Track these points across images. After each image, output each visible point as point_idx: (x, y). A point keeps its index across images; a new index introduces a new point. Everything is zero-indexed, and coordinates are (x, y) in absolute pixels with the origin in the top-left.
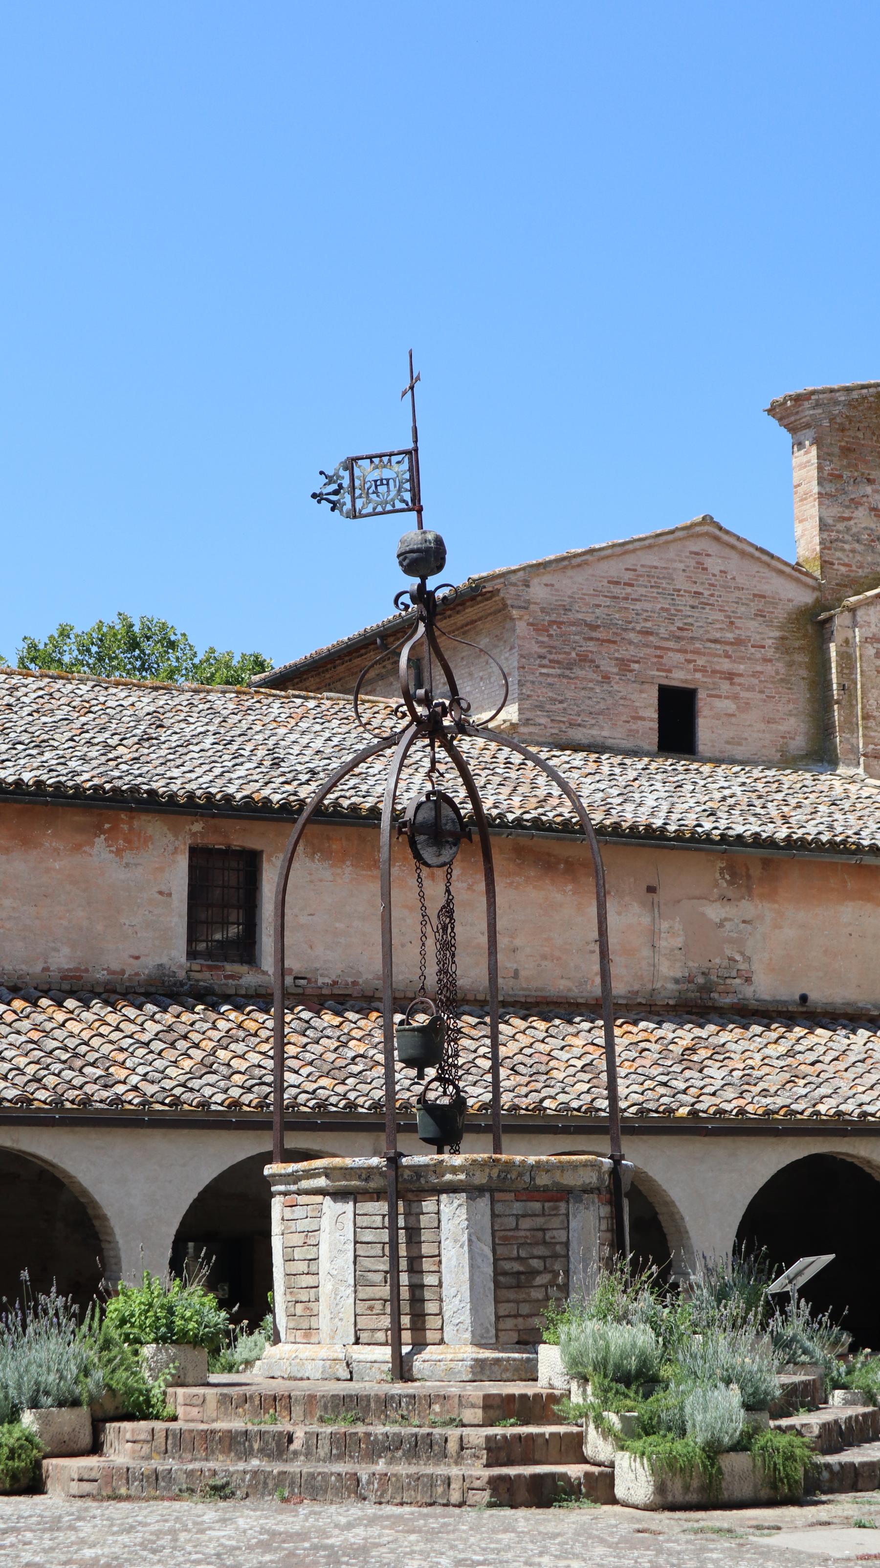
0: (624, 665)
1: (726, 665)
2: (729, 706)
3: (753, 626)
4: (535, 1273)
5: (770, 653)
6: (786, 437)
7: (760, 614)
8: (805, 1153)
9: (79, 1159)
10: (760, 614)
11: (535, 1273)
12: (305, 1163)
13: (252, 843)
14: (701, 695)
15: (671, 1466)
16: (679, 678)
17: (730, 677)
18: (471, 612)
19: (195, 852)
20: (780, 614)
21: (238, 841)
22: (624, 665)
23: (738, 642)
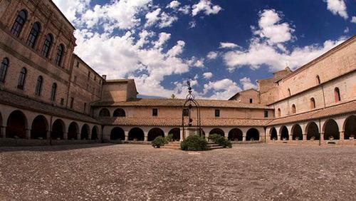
9: (241, 129)
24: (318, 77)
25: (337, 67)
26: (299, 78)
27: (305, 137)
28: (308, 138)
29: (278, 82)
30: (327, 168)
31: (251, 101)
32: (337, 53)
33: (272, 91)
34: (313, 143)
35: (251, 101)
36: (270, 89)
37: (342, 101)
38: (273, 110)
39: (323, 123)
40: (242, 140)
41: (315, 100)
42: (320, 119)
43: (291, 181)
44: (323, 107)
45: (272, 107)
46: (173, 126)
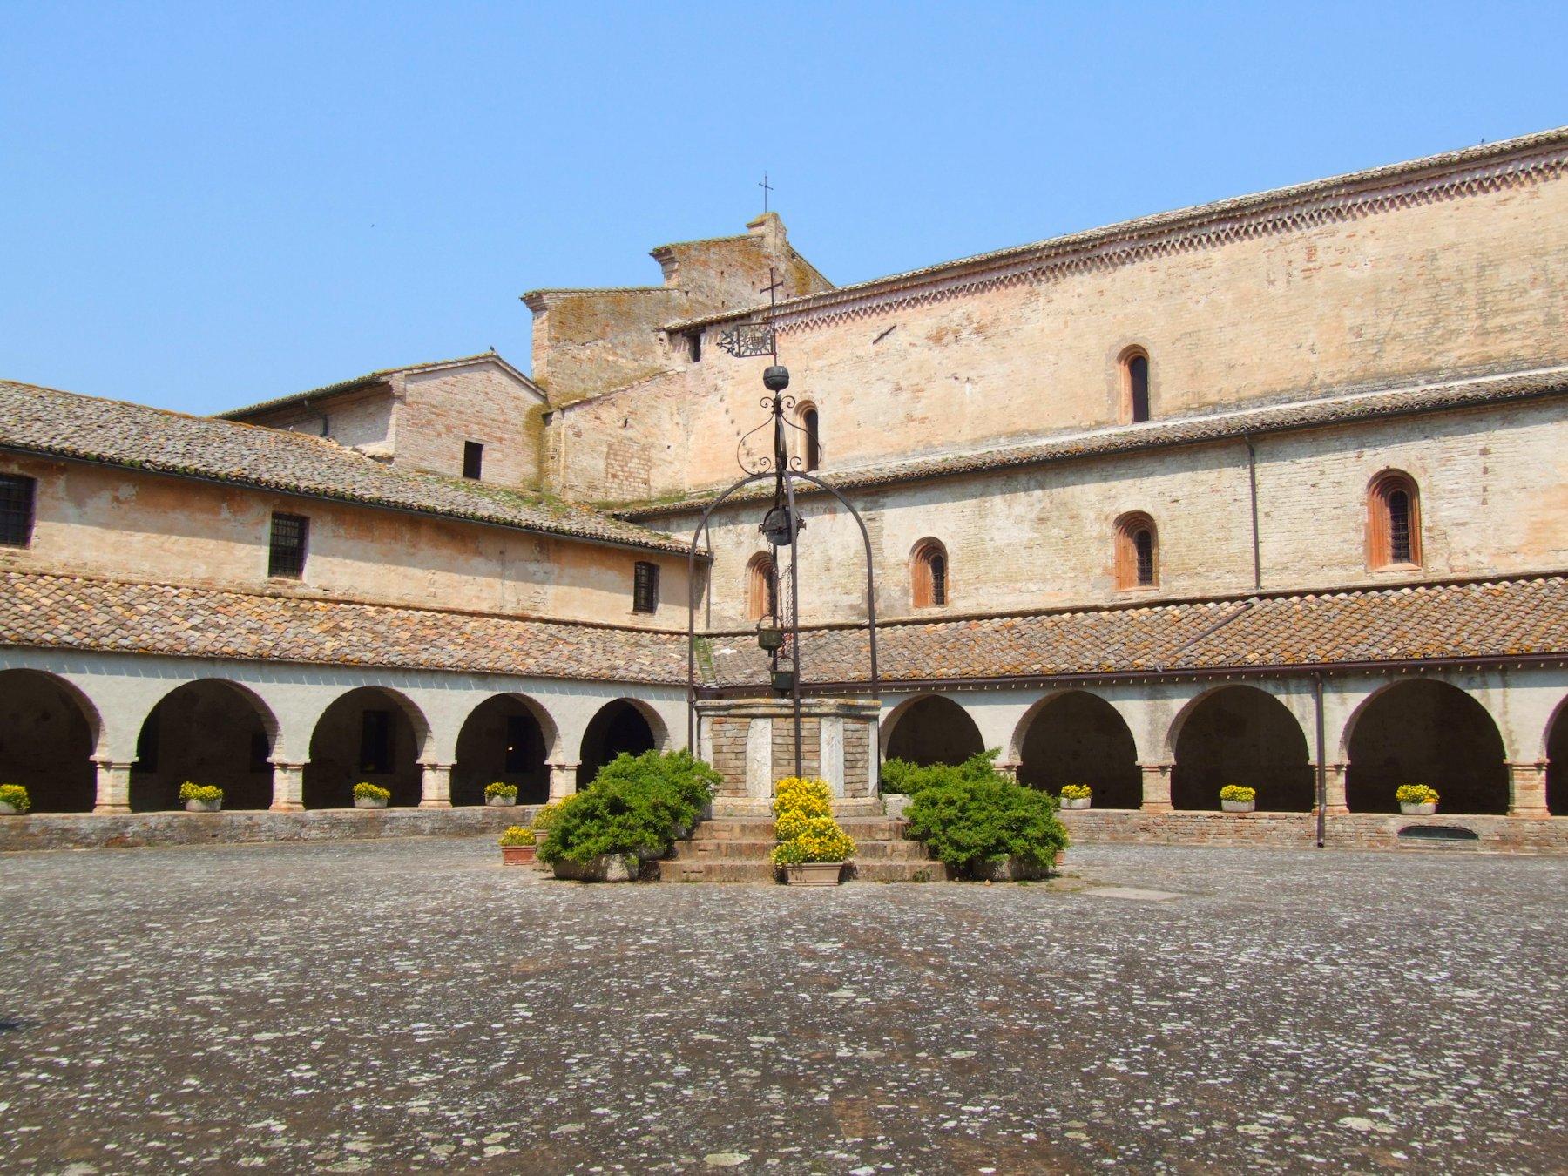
0: (449, 429)
1: (499, 434)
2: (498, 455)
3: (514, 414)
4: (857, 760)
5: (520, 429)
6: (529, 312)
7: (517, 408)
8: (613, 699)
10: (517, 408)
11: (857, 760)
12: (26, 666)
13: (304, 513)
14: (485, 449)
15: (1056, 839)
16: (474, 439)
17: (501, 440)
18: (367, 392)
19: (275, 516)
20: (528, 408)
21: (297, 512)
22: (449, 429)
23: (505, 421)
24: (1137, 362)
25: (1350, 318)
26: (937, 338)
27: (1157, 789)
28: (1194, 791)
29: (692, 336)
30: (753, 1014)
31: (473, 454)
32: (1374, 219)
33: (642, 394)
34: (1242, 843)
35: (473, 454)
36: (628, 383)
37: (959, 602)
38: (700, 565)
39: (1343, 707)
40: (86, 800)
41: (1165, 535)
42: (1322, 677)
43: (1257, 1147)
44: (1245, 584)
45: (683, 537)
46: (1217, 673)
